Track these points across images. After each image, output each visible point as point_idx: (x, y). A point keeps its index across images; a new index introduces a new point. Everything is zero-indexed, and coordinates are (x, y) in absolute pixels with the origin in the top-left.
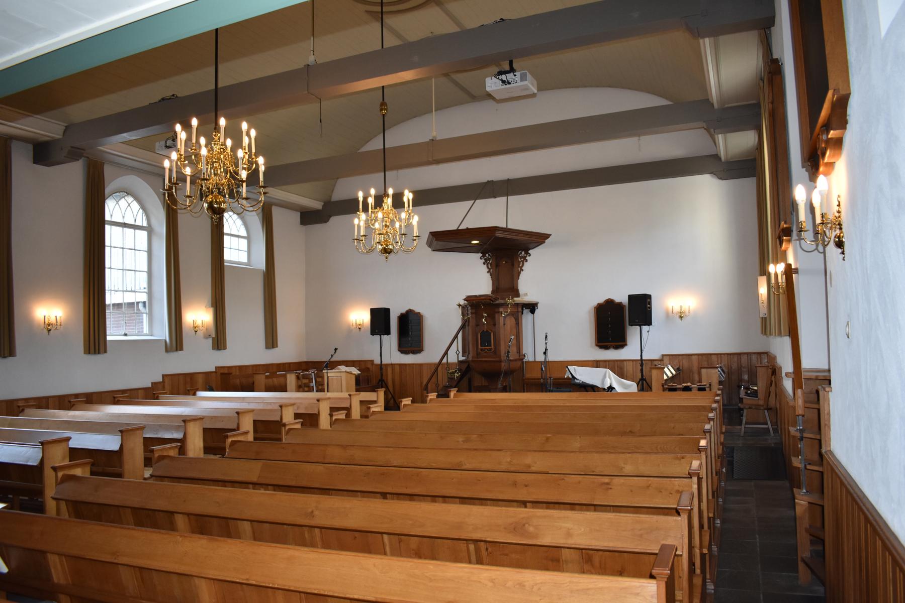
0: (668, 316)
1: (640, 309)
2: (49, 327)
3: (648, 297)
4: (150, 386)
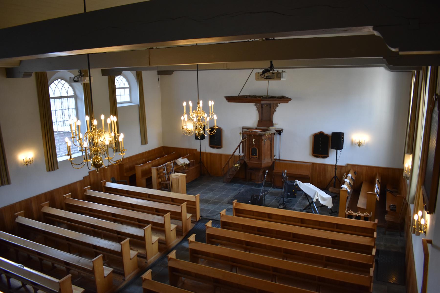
0: (352, 144)
1: (336, 141)
2: (27, 164)
3: (343, 134)
4: (83, 179)
